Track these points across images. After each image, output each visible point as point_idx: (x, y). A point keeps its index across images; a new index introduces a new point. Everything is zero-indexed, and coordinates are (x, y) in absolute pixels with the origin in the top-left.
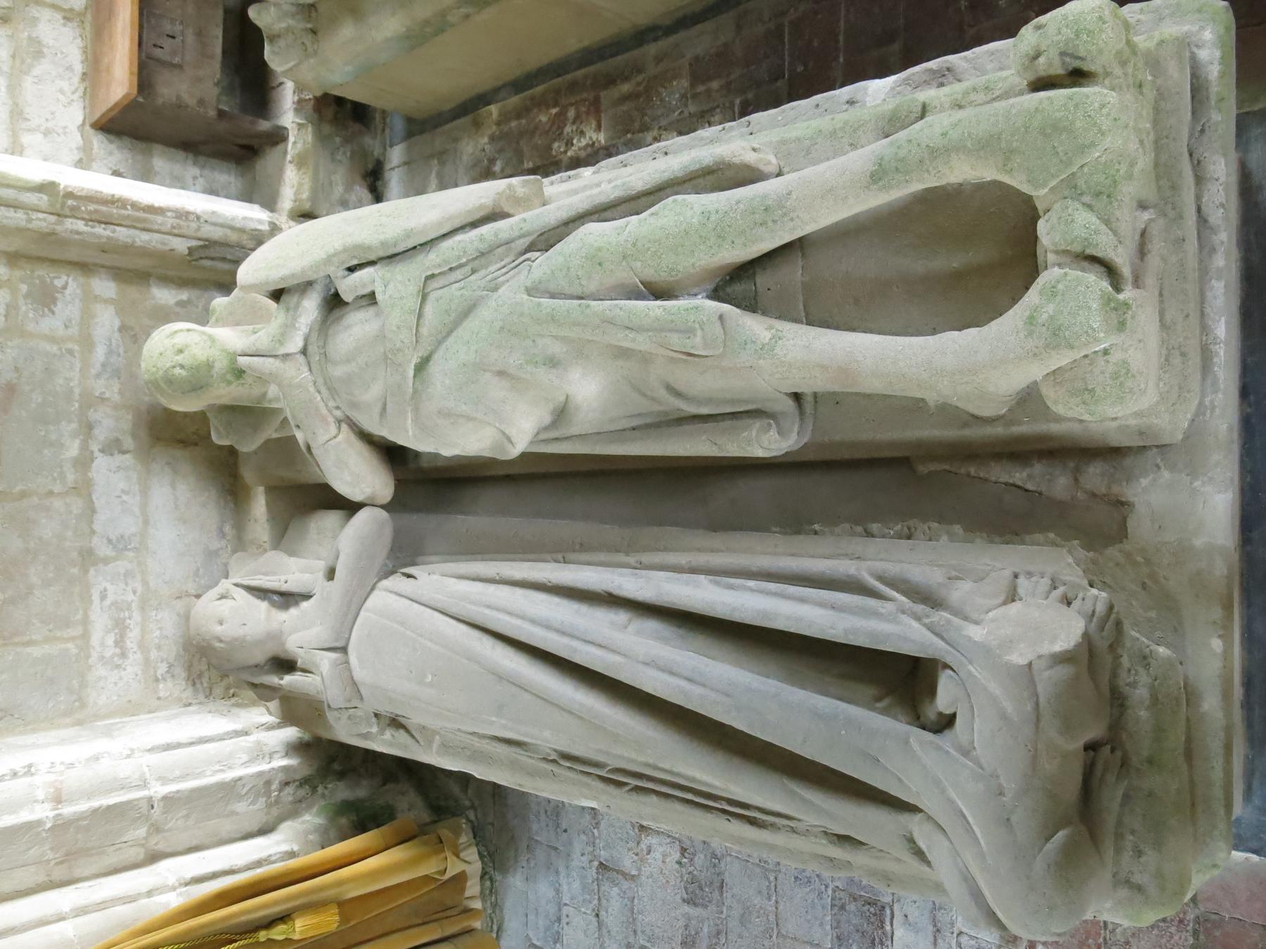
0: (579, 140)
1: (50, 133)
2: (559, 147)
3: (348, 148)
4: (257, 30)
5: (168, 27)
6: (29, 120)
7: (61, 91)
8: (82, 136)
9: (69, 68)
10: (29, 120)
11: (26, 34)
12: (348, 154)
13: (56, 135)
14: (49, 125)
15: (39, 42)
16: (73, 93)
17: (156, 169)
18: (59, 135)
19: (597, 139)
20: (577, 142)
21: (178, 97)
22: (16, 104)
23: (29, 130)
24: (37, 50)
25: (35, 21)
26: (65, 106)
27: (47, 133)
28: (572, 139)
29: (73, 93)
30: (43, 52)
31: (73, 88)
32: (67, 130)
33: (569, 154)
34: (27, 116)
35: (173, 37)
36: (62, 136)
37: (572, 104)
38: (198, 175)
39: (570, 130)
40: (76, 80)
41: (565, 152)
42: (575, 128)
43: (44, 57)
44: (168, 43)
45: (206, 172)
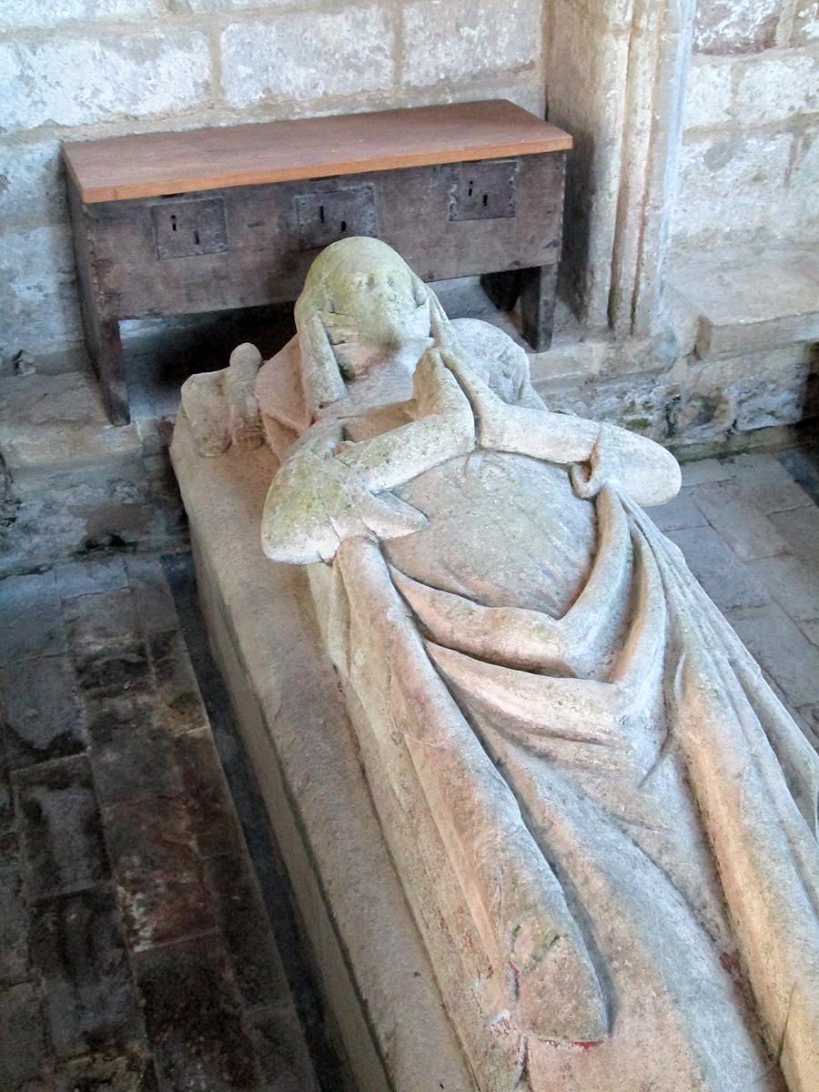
0: (141, 903)
1: (27, 84)
2: (132, 868)
3: (142, 499)
4: (224, 363)
5: (209, 232)
6: (35, 53)
7: (96, 92)
8: (40, 126)
9: (135, 99)
10: (35, 53)
11: (163, 36)
12: (129, 501)
13: (27, 90)
14: (40, 83)
15: (156, 56)
16: (101, 107)
17: (32, 234)
18: (28, 95)
19: (142, 938)
20: (139, 901)
21: (109, 262)
22: (51, 32)
23: (19, 54)
24: (147, 52)
25: (185, 45)
26: (76, 99)
27: (25, 79)
28: (143, 891)
29: (101, 107)
30: (143, 62)
31: (108, 106)
32: (40, 106)
33: (120, 889)
34: (39, 51)
35: (198, 242)
36: (29, 100)
37: (200, 877)
38: (46, 292)
39: (159, 881)
40: (122, 108)
41: (122, 883)
42: (162, 890)
43: (138, 63)
44: (184, 234)
45: (55, 301)
